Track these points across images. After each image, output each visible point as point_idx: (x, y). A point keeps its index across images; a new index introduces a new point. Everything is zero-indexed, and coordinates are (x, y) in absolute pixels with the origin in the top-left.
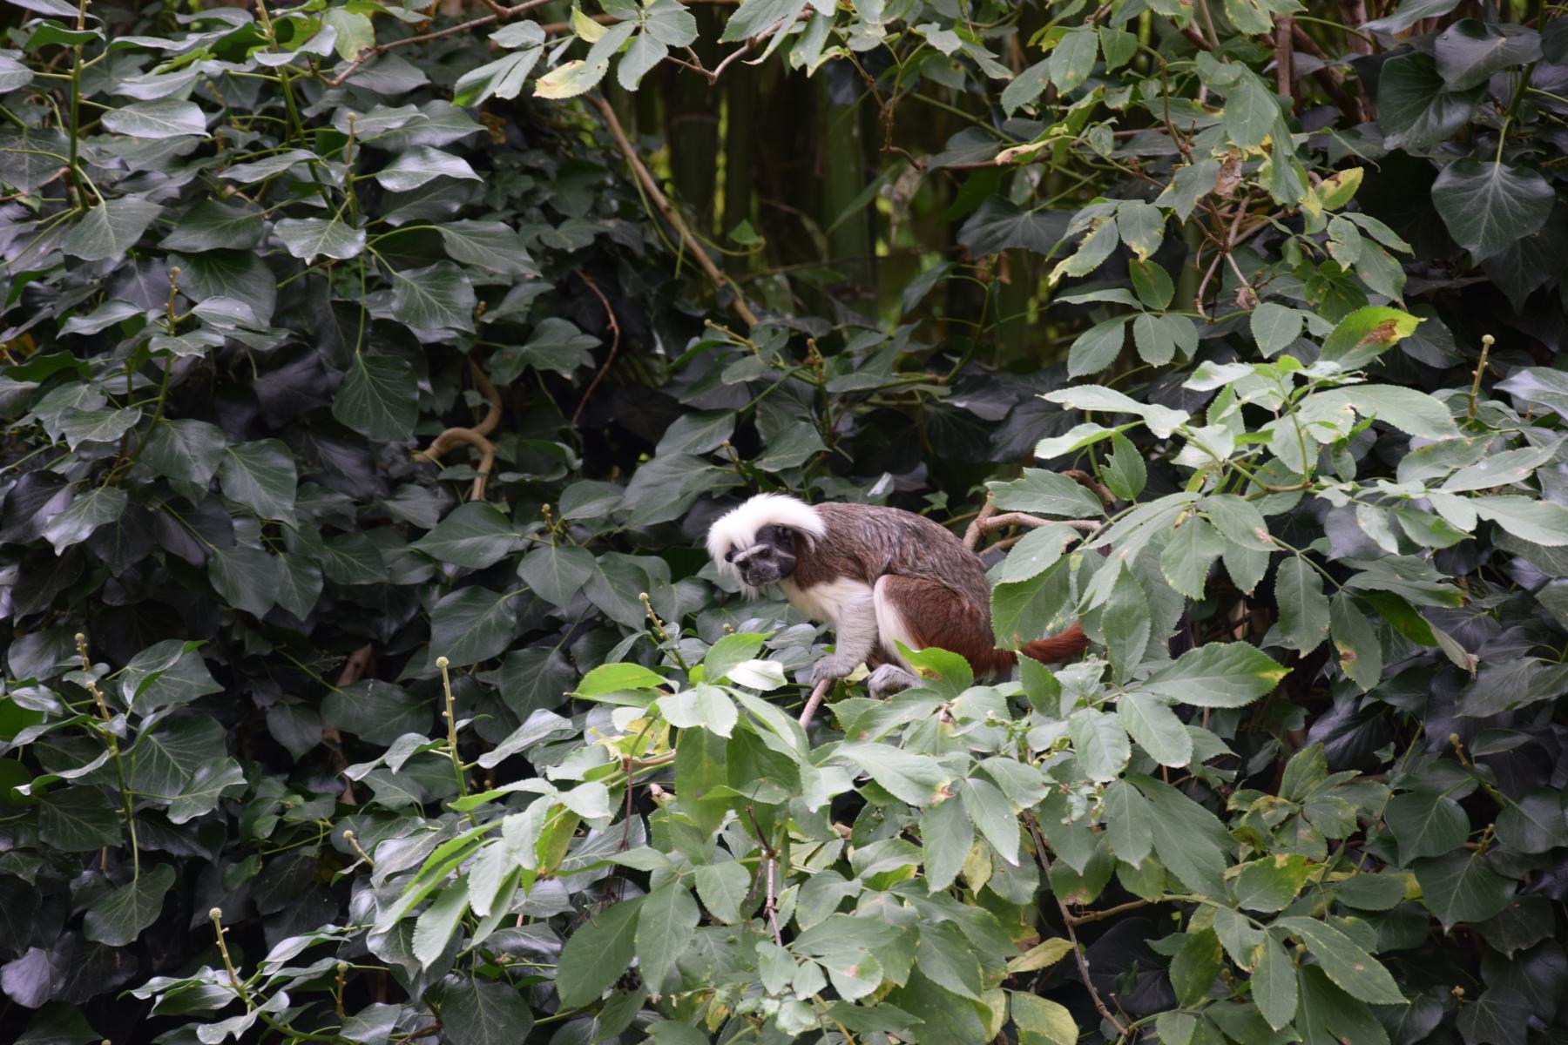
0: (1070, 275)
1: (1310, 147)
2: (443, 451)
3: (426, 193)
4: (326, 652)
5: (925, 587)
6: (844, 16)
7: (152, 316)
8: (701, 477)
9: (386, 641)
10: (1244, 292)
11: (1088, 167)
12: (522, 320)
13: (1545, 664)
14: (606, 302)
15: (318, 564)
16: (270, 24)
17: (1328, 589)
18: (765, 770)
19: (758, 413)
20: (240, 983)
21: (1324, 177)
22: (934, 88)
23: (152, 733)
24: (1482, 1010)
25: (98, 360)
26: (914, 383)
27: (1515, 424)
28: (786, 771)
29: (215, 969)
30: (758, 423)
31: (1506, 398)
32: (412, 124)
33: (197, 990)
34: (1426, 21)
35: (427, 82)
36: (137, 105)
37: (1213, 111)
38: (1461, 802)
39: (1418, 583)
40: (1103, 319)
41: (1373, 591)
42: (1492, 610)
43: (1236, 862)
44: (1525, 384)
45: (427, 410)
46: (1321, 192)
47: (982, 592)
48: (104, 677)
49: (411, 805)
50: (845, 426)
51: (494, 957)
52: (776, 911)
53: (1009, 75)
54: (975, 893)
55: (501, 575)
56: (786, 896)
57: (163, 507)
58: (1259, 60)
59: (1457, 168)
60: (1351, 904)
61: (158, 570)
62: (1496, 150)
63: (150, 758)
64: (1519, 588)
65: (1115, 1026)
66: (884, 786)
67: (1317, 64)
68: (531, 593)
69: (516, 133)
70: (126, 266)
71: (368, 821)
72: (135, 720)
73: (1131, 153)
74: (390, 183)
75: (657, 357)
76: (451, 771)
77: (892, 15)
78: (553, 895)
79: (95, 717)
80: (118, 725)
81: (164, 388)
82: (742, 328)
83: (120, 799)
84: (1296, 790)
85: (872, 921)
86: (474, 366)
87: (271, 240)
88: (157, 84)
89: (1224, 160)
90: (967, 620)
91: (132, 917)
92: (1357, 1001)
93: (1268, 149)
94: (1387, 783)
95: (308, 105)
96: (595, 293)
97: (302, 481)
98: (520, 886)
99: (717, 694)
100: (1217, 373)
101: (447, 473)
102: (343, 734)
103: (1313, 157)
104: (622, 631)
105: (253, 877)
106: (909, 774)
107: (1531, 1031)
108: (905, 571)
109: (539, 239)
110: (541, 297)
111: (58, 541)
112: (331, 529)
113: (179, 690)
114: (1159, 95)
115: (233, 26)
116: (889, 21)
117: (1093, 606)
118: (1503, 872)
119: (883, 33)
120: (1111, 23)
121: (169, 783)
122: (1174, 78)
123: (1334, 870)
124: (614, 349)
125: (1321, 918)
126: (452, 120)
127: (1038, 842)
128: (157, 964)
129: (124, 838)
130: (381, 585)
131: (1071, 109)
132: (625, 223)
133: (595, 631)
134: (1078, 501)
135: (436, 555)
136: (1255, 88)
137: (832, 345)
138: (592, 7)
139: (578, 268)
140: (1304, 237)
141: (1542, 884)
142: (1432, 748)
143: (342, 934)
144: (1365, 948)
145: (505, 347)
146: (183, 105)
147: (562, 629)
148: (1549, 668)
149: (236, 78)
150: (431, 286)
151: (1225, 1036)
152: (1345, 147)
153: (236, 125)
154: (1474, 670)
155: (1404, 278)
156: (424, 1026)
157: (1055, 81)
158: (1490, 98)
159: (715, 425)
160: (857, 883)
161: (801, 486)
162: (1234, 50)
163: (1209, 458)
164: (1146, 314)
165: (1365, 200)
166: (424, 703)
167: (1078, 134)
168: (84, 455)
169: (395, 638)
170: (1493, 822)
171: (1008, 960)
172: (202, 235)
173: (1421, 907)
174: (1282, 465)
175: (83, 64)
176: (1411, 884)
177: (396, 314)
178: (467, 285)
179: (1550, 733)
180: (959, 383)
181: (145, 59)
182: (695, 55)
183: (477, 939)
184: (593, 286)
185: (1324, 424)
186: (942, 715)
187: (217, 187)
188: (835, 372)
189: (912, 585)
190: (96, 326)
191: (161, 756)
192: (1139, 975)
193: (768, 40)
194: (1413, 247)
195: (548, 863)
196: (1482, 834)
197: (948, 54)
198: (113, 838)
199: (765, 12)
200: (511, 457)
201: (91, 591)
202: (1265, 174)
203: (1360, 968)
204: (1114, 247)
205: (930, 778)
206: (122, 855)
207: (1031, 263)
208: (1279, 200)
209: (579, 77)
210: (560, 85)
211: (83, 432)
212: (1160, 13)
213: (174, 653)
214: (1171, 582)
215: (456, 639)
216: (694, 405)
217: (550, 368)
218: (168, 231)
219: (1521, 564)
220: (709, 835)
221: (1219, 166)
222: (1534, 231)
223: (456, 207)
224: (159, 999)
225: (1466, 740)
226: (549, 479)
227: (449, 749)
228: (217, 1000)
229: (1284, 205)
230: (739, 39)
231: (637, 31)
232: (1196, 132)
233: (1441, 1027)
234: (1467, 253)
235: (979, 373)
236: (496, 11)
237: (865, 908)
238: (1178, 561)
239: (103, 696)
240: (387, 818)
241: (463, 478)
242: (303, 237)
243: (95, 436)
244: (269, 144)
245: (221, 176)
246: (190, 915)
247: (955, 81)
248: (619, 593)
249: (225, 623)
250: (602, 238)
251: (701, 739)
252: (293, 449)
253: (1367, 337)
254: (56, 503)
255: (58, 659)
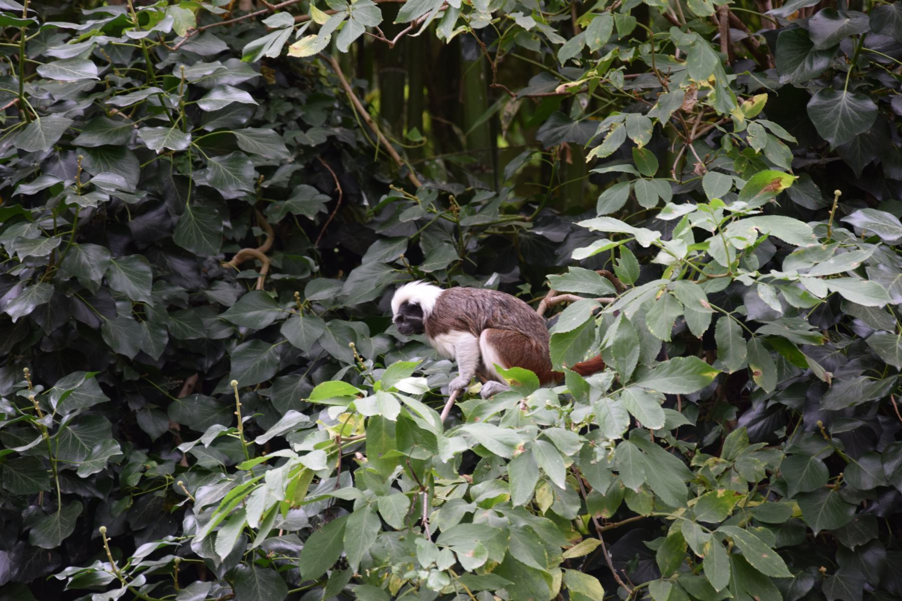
0: (598, 156)
1: (739, 83)
2: (240, 261)
3: (227, 113)
4: (171, 378)
5: (509, 335)
6: (467, 8)
7: (67, 183)
8: (387, 276)
9: (206, 372)
10: (699, 166)
11: (611, 95)
12: (285, 186)
13: (872, 380)
14: (334, 175)
15: (166, 327)
16: (135, 14)
17: (747, 336)
18: (418, 441)
19: (421, 238)
20: (117, 570)
21: (746, 99)
22: (522, 51)
23: (68, 425)
24: (837, 580)
25: (37, 210)
26: (512, 220)
27: (853, 242)
28: (429, 440)
29: (103, 562)
30: (421, 245)
31: (850, 227)
32: (218, 72)
33: (92, 575)
34: (807, 9)
35: (228, 48)
36: (58, 62)
37: (681, 62)
38: (825, 461)
39: (798, 331)
40: (622, 181)
41: (772, 336)
42: (843, 349)
43: (696, 496)
44: (859, 218)
45: (230, 238)
46: (743, 109)
47: (544, 337)
48: (40, 393)
49: (219, 466)
50: (472, 245)
51: (265, 554)
52: (428, 523)
53: (564, 41)
54: (544, 513)
55: (271, 333)
56: (434, 515)
57: (75, 294)
58: (708, 32)
59: (822, 94)
60: (761, 520)
61: (73, 331)
62: (845, 84)
63: (68, 440)
64: (858, 337)
65: (627, 591)
66: (486, 446)
67: (744, 35)
68: (288, 343)
69: (282, 78)
70: (54, 155)
71: (194, 476)
72: (58, 417)
73: (638, 86)
74: (205, 106)
75: (364, 207)
76: (241, 446)
77: (494, 8)
78: (299, 518)
79: (36, 417)
80: (48, 421)
81: (75, 226)
82: (411, 189)
83: (49, 464)
84: (731, 454)
85: (483, 526)
86: (258, 212)
87: (138, 140)
88: (70, 50)
89: (687, 90)
90: (535, 352)
91: (57, 533)
92: (764, 575)
93: (713, 83)
94: (782, 450)
95: (161, 61)
96: (328, 170)
97: (156, 280)
98: (280, 512)
99: (388, 396)
100: (676, 210)
101: (241, 275)
102: (182, 426)
103: (740, 89)
104: (341, 364)
105: (128, 509)
106: (500, 440)
107: (865, 593)
108: (497, 325)
109: (294, 139)
110: (296, 173)
111: (13, 314)
112: (173, 307)
113: (84, 400)
114: (650, 53)
115: (114, 16)
116: (493, 11)
117: (607, 346)
118: (849, 500)
119: (491, 18)
120: (621, 10)
121: (78, 454)
122: (659, 43)
123: (751, 500)
124: (339, 202)
125: (745, 528)
126: (242, 69)
127: (581, 483)
128: (72, 559)
129: (52, 486)
130: (203, 340)
131: (599, 61)
132: (345, 130)
133: (326, 365)
134: (600, 286)
135: (234, 322)
136: (705, 49)
137: (465, 199)
138: (322, 6)
139: (318, 156)
140: (734, 134)
141: (872, 508)
142: (808, 429)
143: (178, 541)
144: (769, 545)
145: (275, 202)
146: (84, 62)
147: (308, 364)
148: (874, 382)
149: (118, 46)
150: (229, 166)
151: (689, 595)
152: (758, 83)
153: (118, 74)
154: (830, 382)
155: (792, 156)
156: (227, 594)
157: (589, 44)
158: (841, 54)
159: (396, 246)
160: (474, 505)
161: (446, 281)
162: (693, 27)
163: (674, 259)
164: (642, 179)
165: (770, 112)
166: (228, 407)
167: (603, 76)
168: (29, 264)
169: (211, 370)
170: (843, 472)
171: (564, 550)
172: (96, 137)
173: (801, 521)
174: (717, 264)
175: (26, 38)
176: (796, 508)
177: (209, 182)
178: (250, 165)
179: (876, 420)
180: (539, 220)
181: (66, 36)
182: (381, 32)
183: (256, 544)
184: (327, 166)
185: (739, 238)
186: (521, 405)
187: (106, 110)
188: (466, 214)
189: (502, 334)
190: (35, 190)
191: (74, 439)
192: (640, 562)
193: (423, 22)
194: (797, 139)
195: (296, 499)
196: (836, 479)
197: (528, 29)
198: (45, 487)
199: (420, 6)
200: (279, 265)
201: (34, 343)
202: (711, 98)
203: (765, 556)
204: (623, 141)
205: (512, 441)
206: (52, 496)
207: (579, 150)
208: (720, 111)
209: (314, 44)
210: (303, 49)
211: (28, 251)
212: (649, 4)
213: (81, 379)
214: (652, 331)
215: (245, 370)
216: (386, 234)
217: (301, 213)
218: (78, 134)
219: (858, 322)
220: (387, 479)
221: (684, 93)
222: (866, 130)
223: (244, 120)
224: (70, 579)
225: (826, 424)
226: (300, 277)
227: (238, 433)
228: (104, 580)
229: (723, 114)
230: (406, 22)
231: (347, 18)
232: (672, 74)
233: (813, 589)
234: (828, 144)
235: (549, 214)
236: (268, 7)
237: (477, 519)
238: (656, 319)
239: (39, 404)
240: (205, 474)
241: (251, 277)
242: (154, 137)
243: (34, 253)
244: (137, 85)
245: (107, 103)
246: (91, 531)
247: (535, 46)
248: (339, 343)
249: (112, 362)
250: (332, 138)
251: (381, 424)
252: (151, 261)
253: (765, 188)
254: (12, 293)
255: (15, 383)
